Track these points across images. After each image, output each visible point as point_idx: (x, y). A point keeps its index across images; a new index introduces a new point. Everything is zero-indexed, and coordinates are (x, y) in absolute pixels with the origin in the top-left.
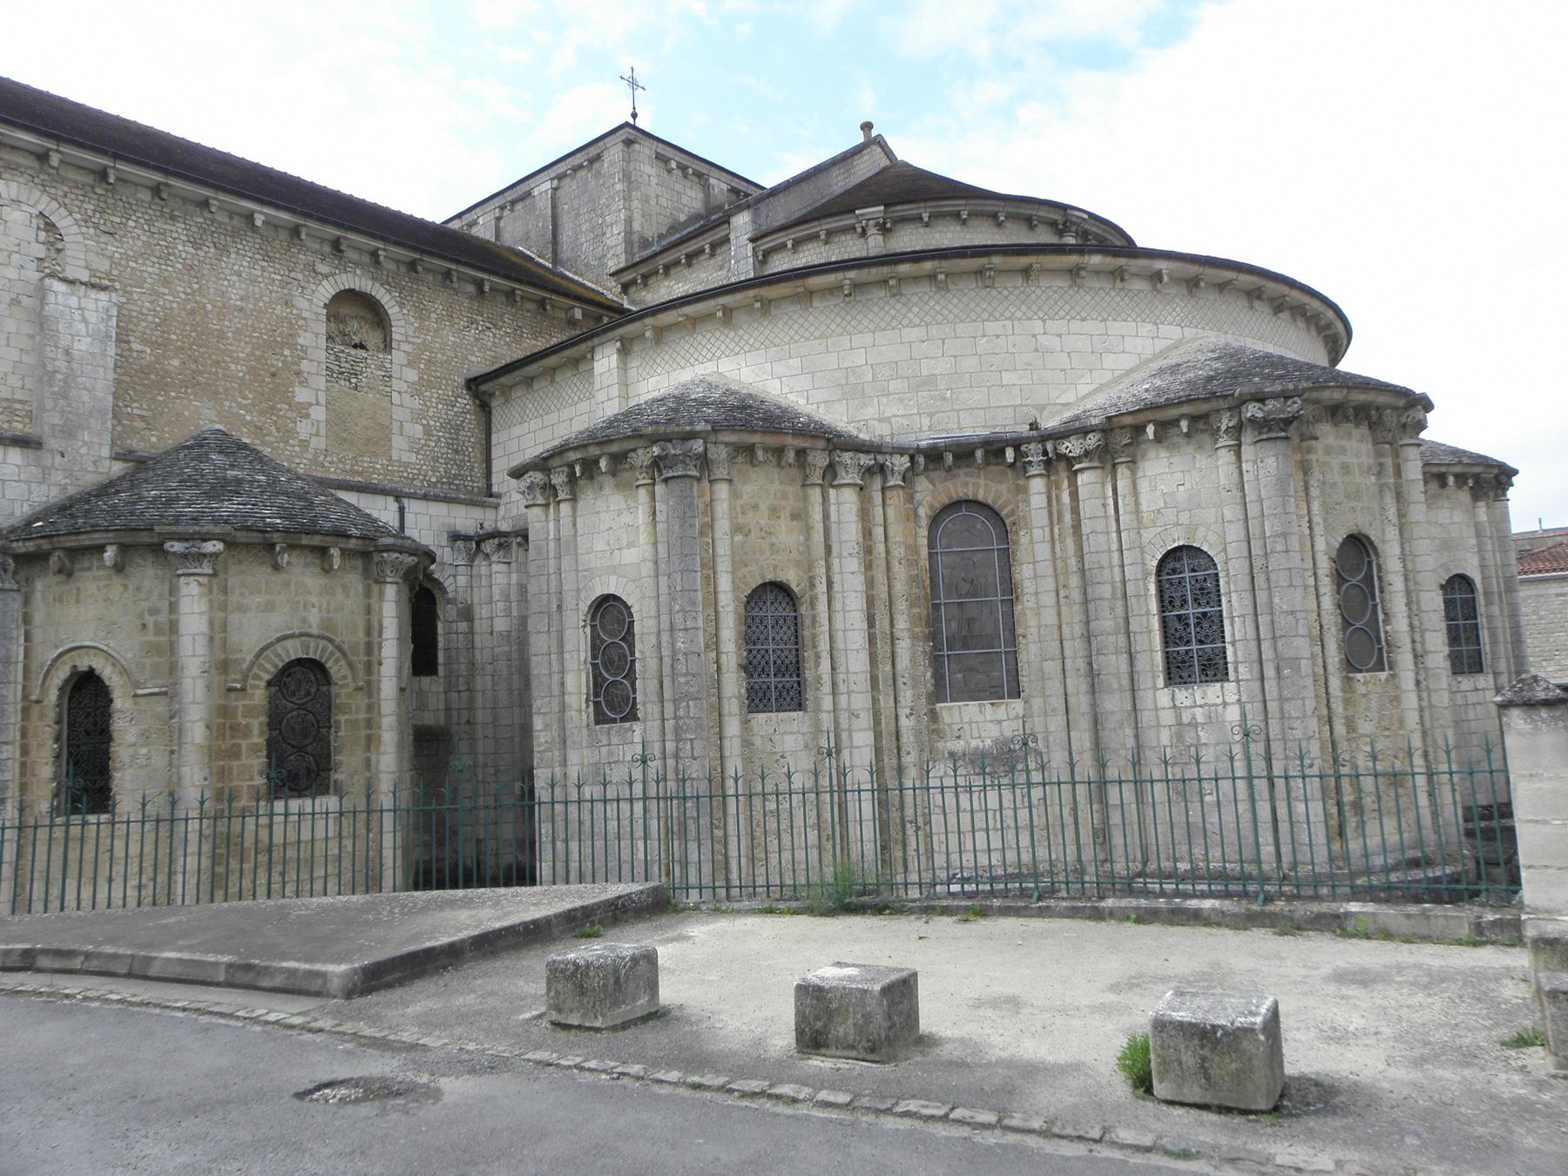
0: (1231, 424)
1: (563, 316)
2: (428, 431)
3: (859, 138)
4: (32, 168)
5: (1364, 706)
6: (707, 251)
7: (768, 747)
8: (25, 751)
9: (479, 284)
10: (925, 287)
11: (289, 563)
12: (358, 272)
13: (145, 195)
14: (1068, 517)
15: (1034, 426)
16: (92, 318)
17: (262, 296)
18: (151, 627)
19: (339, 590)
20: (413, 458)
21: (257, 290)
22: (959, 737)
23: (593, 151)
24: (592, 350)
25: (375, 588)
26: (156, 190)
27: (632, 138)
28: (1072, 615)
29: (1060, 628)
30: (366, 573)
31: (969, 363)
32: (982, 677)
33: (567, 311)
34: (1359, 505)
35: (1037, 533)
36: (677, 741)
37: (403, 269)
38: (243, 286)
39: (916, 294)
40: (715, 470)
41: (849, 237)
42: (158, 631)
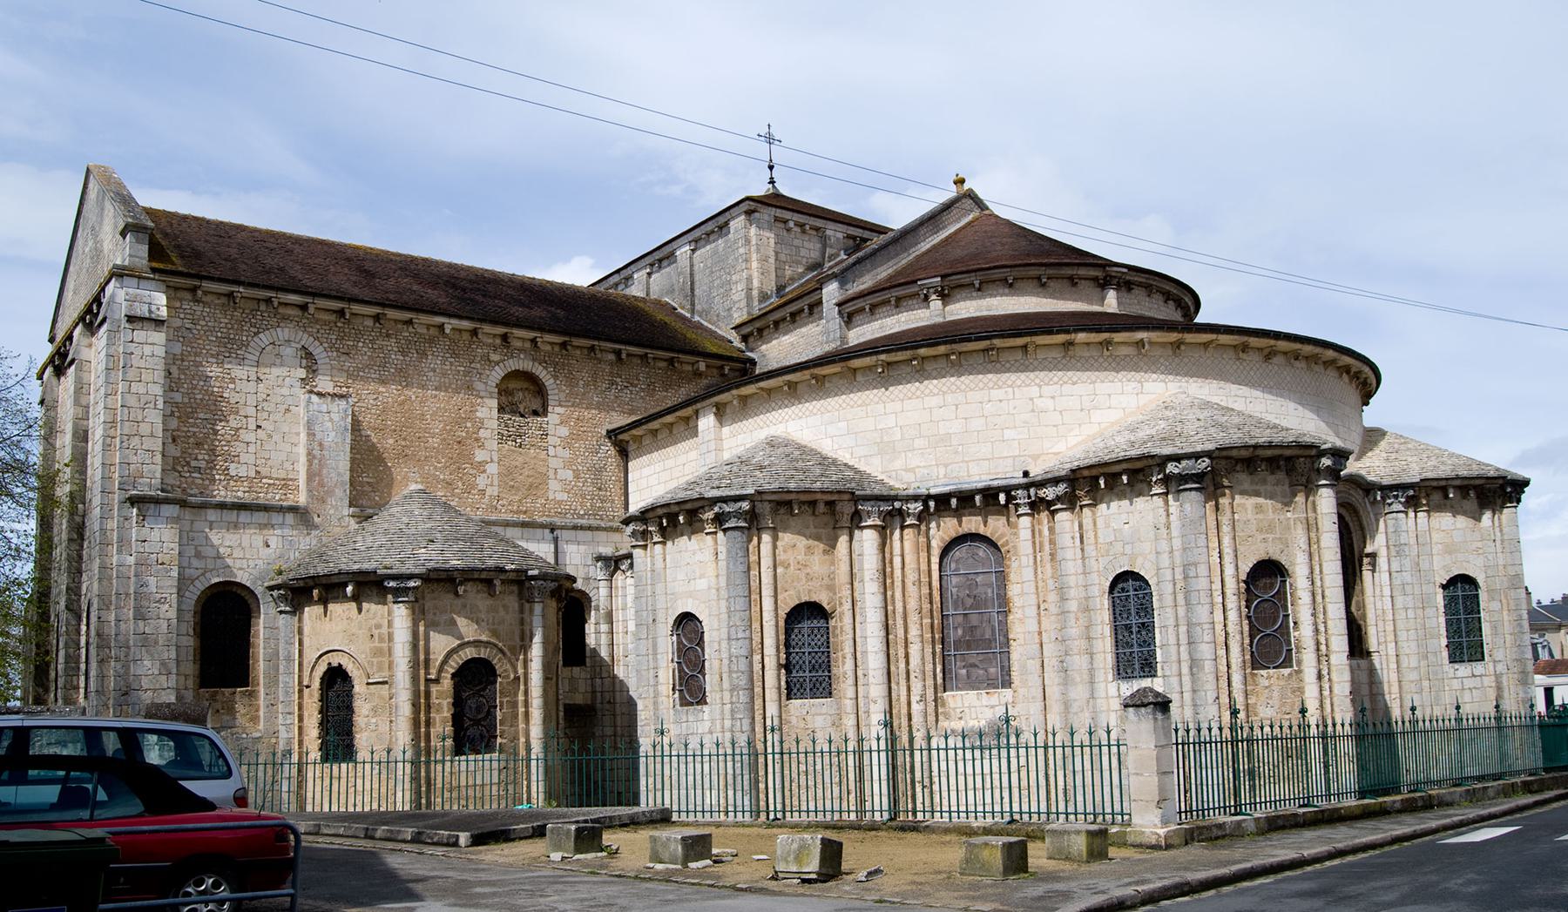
0: (1159, 477)
1: (690, 369)
2: (577, 477)
3: (951, 192)
4: (298, 316)
5: (1266, 696)
6: (806, 311)
7: (802, 724)
8: (301, 719)
9: (618, 353)
10: (942, 363)
11: (465, 591)
12: (522, 356)
13: (369, 322)
14: (1047, 547)
15: (1026, 474)
16: (335, 417)
17: (450, 384)
18: (376, 637)
19: (501, 609)
20: (565, 496)
21: (447, 380)
22: (961, 718)
23: (721, 220)
24: (697, 413)
25: (527, 606)
26: (377, 318)
27: (752, 208)
28: (1049, 624)
29: (1040, 633)
30: (520, 595)
31: (977, 424)
32: (981, 672)
33: (693, 364)
34: (1270, 536)
35: (1024, 559)
36: (733, 719)
37: (557, 349)
38: (437, 379)
39: (936, 369)
40: (762, 521)
41: (915, 302)
42: (381, 640)
